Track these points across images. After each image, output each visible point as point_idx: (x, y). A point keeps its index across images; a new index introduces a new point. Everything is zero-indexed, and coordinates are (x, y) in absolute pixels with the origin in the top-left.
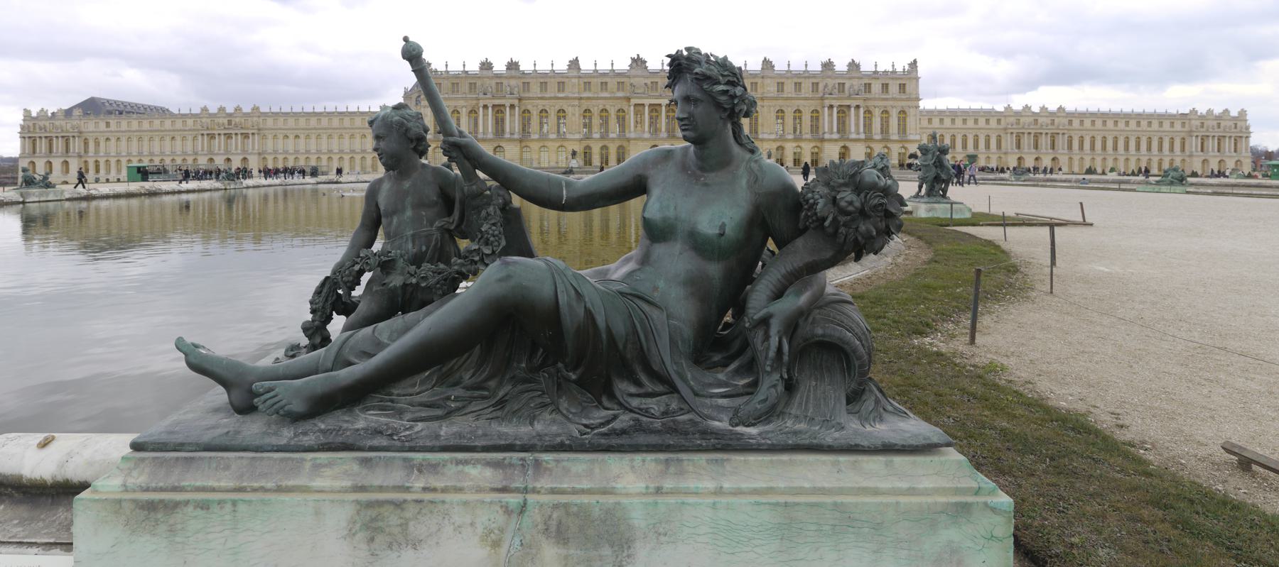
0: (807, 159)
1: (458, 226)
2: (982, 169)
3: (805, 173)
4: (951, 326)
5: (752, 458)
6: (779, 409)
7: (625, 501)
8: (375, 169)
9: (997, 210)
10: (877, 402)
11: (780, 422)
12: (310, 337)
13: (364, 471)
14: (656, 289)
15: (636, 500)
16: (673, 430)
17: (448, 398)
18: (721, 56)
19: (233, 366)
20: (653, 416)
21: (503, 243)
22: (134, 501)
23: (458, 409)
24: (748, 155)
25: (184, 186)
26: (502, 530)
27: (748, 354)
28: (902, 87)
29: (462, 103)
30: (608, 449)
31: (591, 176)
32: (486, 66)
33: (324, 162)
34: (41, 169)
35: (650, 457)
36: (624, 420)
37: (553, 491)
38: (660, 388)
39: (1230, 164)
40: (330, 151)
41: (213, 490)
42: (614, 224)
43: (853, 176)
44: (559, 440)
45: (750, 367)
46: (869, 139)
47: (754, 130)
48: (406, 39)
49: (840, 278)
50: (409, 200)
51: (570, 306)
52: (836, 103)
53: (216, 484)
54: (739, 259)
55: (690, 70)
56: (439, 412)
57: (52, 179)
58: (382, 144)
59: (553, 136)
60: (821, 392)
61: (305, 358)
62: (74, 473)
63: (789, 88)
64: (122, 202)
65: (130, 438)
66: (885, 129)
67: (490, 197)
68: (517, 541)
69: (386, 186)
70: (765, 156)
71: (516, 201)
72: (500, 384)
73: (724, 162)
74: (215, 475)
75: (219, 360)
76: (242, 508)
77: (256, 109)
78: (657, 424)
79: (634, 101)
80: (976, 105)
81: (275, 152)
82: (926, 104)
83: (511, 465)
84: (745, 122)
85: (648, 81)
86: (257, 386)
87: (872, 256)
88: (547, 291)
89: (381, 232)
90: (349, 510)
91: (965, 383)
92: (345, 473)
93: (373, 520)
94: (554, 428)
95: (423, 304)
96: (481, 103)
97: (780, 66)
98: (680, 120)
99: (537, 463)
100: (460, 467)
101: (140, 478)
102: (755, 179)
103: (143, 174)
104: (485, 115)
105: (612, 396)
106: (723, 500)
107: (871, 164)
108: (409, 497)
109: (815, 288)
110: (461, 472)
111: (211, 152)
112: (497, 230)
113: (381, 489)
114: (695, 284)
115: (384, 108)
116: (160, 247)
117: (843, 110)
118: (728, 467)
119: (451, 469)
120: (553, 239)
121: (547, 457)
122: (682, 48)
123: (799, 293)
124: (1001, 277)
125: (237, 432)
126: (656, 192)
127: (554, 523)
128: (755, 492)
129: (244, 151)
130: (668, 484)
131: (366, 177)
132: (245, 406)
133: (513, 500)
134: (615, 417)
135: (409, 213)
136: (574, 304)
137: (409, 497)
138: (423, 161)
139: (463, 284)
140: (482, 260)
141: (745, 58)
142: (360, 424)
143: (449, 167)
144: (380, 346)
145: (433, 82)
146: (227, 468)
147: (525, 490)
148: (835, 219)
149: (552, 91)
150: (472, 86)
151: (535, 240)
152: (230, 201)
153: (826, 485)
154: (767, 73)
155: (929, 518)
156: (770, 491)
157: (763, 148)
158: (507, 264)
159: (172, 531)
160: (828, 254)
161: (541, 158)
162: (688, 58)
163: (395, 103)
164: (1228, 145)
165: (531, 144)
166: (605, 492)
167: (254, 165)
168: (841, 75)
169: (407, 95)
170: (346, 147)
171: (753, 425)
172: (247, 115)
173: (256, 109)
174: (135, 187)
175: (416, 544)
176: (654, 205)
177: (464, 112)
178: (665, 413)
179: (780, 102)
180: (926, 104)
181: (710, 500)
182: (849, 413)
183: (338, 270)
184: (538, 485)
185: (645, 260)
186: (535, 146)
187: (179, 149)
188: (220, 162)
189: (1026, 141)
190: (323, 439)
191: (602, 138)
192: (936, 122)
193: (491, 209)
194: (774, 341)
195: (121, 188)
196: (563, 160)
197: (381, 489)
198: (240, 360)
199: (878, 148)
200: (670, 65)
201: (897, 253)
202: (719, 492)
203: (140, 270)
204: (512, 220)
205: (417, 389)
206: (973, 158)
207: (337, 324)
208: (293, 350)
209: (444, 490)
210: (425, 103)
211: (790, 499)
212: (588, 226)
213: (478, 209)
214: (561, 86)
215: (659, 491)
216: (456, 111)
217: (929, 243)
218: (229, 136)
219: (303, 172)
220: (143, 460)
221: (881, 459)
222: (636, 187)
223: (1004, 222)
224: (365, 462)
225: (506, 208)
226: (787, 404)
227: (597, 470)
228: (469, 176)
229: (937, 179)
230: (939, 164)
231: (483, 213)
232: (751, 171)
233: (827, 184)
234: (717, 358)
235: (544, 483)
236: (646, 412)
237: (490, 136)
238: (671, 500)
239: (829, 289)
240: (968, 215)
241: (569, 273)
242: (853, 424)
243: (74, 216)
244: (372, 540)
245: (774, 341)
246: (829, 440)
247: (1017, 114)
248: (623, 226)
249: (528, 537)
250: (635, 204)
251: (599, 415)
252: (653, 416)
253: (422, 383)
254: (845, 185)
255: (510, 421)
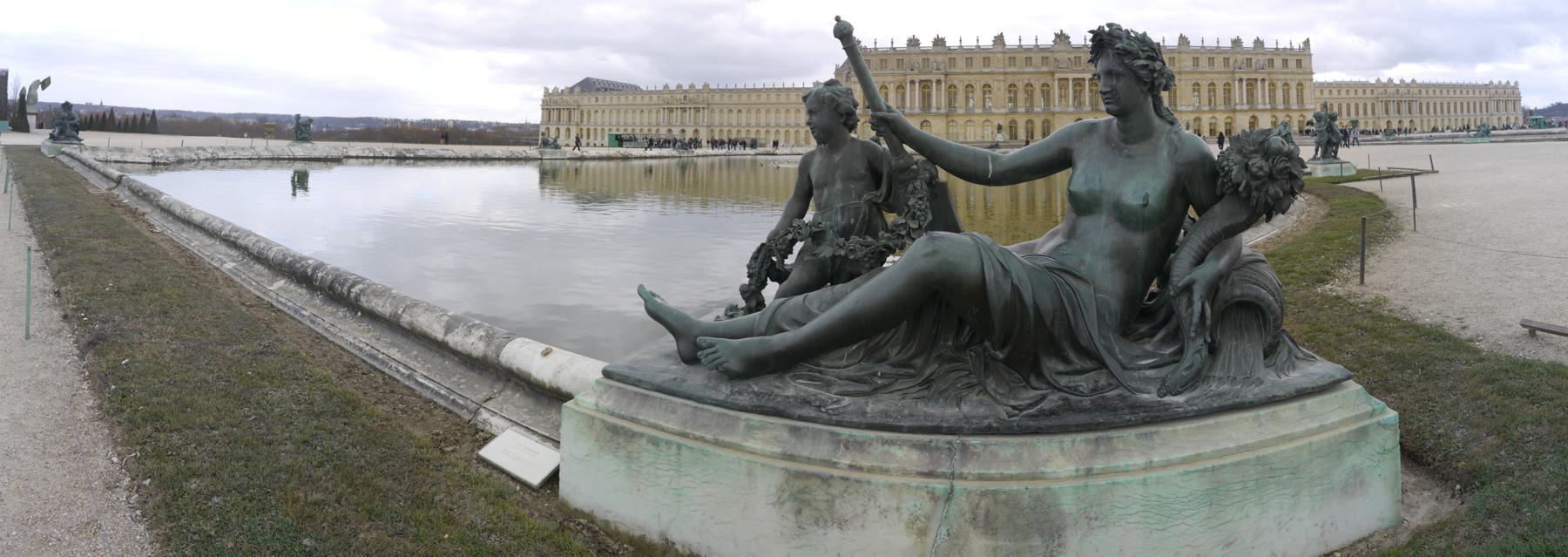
0: (1221, 129)
1: (886, 200)
2: (1362, 132)
3: (1221, 143)
4: (1345, 271)
5: (1180, 427)
6: (1204, 373)
7: (1055, 486)
8: (807, 142)
9: (1374, 166)
10: (1290, 351)
11: (1205, 387)
12: (746, 300)
13: (793, 440)
14: (1082, 262)
15: (1066, 485)
16: (1102, 407)
17: (875, 374)
18: (1140, 32)
19: (683, 318)
20: (1082, 394)
21: (930, 217)
22: (603, 421)
23: (885, 386)
24: (1168, 127)
25: (650, 152)
26: (928, 518)
27: (1174, 322)
28: (1299, 62)
29: (889, 78)
30: (1037, 432)
31: (1016, 150)
32: (913, 42)
33: (762, 135)
34: (553, 134)
35: (1080, 437)
36: (1053, 400)
37: (981, 478)
38: (1088, 364)
39: (1512, 120)
40: (768, 125)
41: (662, 429)
42: (1040, 198)
43: (1262, 143)
44: (986, 422)
45: (1176, 335)
46: (1274, 109)
47: (1173, 102)
48: (838, 19)
49: (1254, 239)
50: (839, 173)
51: (996, 282)
52: (1245, 77)
53: (665, 425)
54: (1161, 230)
55: (1111, 45)
56: (866, 388)
57: (560, 142)
58: (815, 118)
59: (979, 111)
60: (1242, 349)
61: (742, 319)
62: (565, 384)
63: (1204, 63)
64: (604, 163)
65: (602, 365)
66: (1286, 100)
67: (917, 172)
68: (944, 531)
69: (817, 159)
70: (1183, 127)
71: (943, 175)
72: (926, 364)
73: (1147, 134)
74: (666, 416)
75: (670, 311)
76: (685, 452)
77: (706, 86)
78: (1087, 402)
79: (1058, 76)
80: (1356, 79)
81: (721, 125)
82: (1318, 77)
83: (938, 448)
84: (1164, 95)
85: (1072, 56)
86: (700, 339)
87: (1280, 216)
88: (972, 266)
89: (812, 203)
90: (776, 479)
91: (1358, 320)
92: (776, 438)
93: (802, 491)
94: (982, 410)
95: (851, 277)
96: (909, 78)
97: (1195, 42)
98: (1103, 93)
99: (965, 448)
100: (886, 447)
101: (608, 403)
102: (1175, 150)
103: (619, 140)
104: (912, 90)
105: (1040, 376)
106: (1153, 475)
107: (1276, 131)
108: (836, 473)
109: (1233, 251)
110: (887, 452)
111: (670, 124)
112: (924, 204)
113: (808, 460)
114: (1121, 256)
115: (816, 84)
116: (629, 204)
117: (1251, 83)
118: (1157, 440)
119: (878, 449)
120: (980, 213)
121: (974, 441)
122: (1103, 24)
123: (1218, 258)
124: (1380, 222)
125: (683, 380)
126: (1081, 165)
127: (982, 512)
128: (1184, 461)
129: (696, 123)
130: (1099, 465)
131: (799, 150)
132: (690, 357)
133: (940, 485)
134: (1044, 397)
135: (839, 186)
136: (1001, 279)
137: (836, 473)
138: (853, 135)
139: (890, 258)
140: (909, 234)
141: (1164, 35)
142: (790, 392)
143: (877, 141)
144: (810, 316)
145: (863, 58)
146: (674, 412)
147: (952, 476)
148: (1248, 184)
149: (978, 66)
150: (900, 62)
151: (961, 215)
152: (683, 167)
153: (1249, 441)
154: (1184, 48)
155: (1335, 451)
156: (1198, 458)
157: (1182, 119)
158: (934, 239)
159: (629, 457)
160: (1243, 217)
161: (967, 132)
162: (1109, 34)
163: (827, 79)
164: (1510, 106)
165: (957, 119)
166: (1034, 477)
167: (703, 136)
168: (1248, 51)
169: (838, 71)
170: (782, 122)
171: (1180, 393)
172: (699, 91)
173: (706, 86)
174: (613, 151)
175: (842, 524)
176: (1080, 178)
177: (892, 87)
178: (1094, 390)
179: (1196, 76)
180: (1318, 77)
181: (1140, 477)
182: (1267, 366)
183: (773, 237)
184: (966, 471)
185: (1071, 234)
186: (961, 121)
187: (646, 120)
188: (676, 132)
189: (1392, 107)
190: (756, 402)
191: (1027, 112)
192: (1326, 92)
193: (918, 183)
194: (1197, 306)
195: (604, 152)
196: (989, 134)
197: (808, 460)
198: (688, 313)
199: (1281, 117)
200: (1093, 40)
201: (1300, 213)
202: (1149, 467)
203: (614, 222)
204: (938, 194)
205: (844, 362)
206: (1355, 123)
207: (771, 290)
208: (732, 311)
209: (870, 470)
210: (855, 79)
211: (1217, 462)
212: (1015, 199)
213: (905, 183)
214: (987, 61)
215: (1089, 473)
216: (884, 87)
217: (1326, 200)
218: (684, 110)
219: (744, 144)
220: (610, 387)
221: (1296, 404)
222: (1061, 160)
223: (1380, 176)
224: (794, 431)
225: (933, 183)
226: (1211, 367)
227: (1026, 455)
228: (896, 150)
229: (1329, 142)
230: (1330, 129)
231: (910, 187)
232: (1171, 142)
233: (1240, 152)
234: (1143, 329)
235: (971, 469)
236: (1075, 390)
237: (917, 111)
238: (1102, 481)
239: (1245, 251)
240: (1354, 172)
241: (996, 249)
242: (1271, 377)
243: (572, 173)
244: (799, 512)
245: (1197, 306)
246: (1250, 397)
247: (1385, 85)
248: (1049, 200)
249: (955, 526)
250: (1061, 177)
251: (1028, 395)
252: (1082, 394)
253: (849, 356)
254: (1255, 152)
255: (937, 402)
